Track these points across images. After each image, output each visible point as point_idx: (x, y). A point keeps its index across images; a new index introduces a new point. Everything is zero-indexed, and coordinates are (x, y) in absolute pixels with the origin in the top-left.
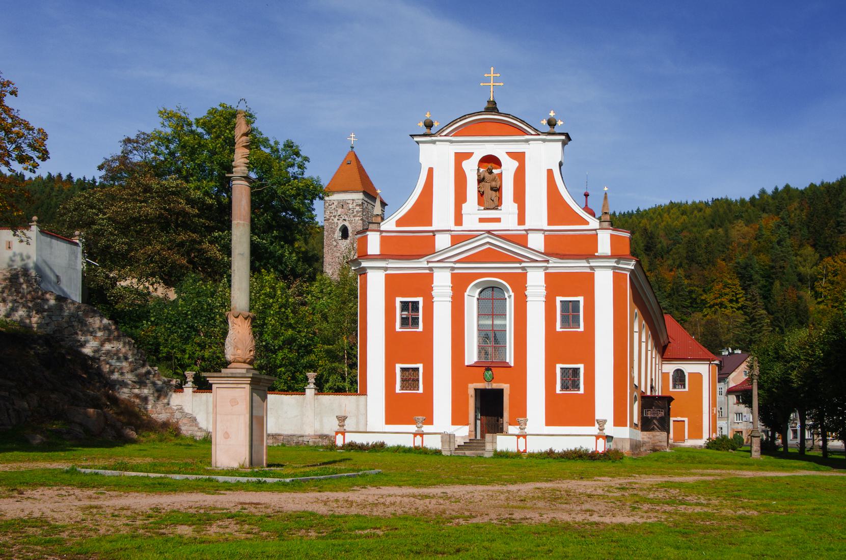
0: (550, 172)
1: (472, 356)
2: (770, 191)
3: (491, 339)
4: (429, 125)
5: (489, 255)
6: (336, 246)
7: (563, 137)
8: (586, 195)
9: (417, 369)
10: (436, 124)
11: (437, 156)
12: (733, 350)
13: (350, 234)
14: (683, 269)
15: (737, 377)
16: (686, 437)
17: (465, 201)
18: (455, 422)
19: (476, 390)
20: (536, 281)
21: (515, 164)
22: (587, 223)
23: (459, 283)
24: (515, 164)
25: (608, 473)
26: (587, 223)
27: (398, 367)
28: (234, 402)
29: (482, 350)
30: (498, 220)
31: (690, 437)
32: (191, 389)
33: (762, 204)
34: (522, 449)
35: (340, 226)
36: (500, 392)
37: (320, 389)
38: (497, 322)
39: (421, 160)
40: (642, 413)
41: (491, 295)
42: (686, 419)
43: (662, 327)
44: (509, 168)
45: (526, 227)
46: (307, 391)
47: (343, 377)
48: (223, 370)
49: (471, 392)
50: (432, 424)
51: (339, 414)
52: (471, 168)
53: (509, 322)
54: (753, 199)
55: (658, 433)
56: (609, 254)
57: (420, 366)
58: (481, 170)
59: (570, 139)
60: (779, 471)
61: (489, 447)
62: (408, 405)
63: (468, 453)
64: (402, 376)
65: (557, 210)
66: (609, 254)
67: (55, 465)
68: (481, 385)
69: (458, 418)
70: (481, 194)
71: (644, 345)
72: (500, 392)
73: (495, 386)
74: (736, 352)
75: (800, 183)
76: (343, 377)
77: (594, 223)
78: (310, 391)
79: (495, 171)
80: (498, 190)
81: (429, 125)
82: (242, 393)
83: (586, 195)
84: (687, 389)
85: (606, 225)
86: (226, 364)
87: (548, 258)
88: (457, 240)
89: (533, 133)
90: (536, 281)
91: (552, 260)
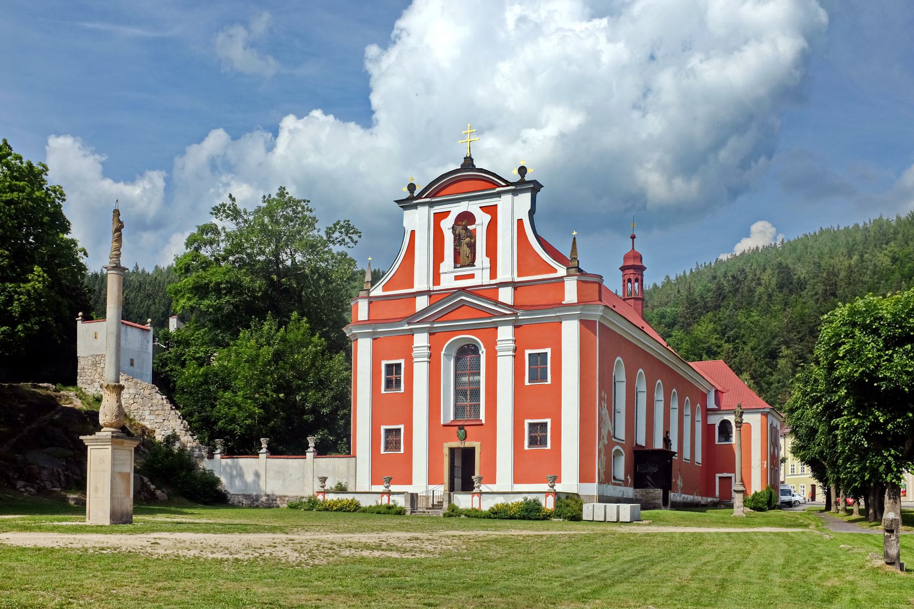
0: (520, 222)
1: (448, 414)
3: (467, 394)
4: (412, 187)
8: (633, 237)
17: (442, 260)
20: (505, 333)
21: (488, 218)
22: (555, 271)
24: (488, 218)
26: (555, 271)
29: (458, 410)
30: (472, 276)
31: (713, 495)
32: (312, 454)
34: (476, 506)
37: (273, 452)
38: (476, 378)
39: (405, 225)
40: (635, 469)
41: (466, 352)
44: (482, 219)
46: (308, 454)
47: (337, 442)
49: (446, 451)
50: (495, 483)
52: (447, 225)
55: (651, 490)
60: (722, 527)
62: (392, 463)
64: (386, 437)
68: (456, 444)
69: (433, 479)
73: (468, 444)
76: (337, 442)
77: (562, 271)
78: (310, 455)
79: (470, 227)
80: (472, 246)
83: (633, 237)
89: (503, 184)
91: (520, 312)
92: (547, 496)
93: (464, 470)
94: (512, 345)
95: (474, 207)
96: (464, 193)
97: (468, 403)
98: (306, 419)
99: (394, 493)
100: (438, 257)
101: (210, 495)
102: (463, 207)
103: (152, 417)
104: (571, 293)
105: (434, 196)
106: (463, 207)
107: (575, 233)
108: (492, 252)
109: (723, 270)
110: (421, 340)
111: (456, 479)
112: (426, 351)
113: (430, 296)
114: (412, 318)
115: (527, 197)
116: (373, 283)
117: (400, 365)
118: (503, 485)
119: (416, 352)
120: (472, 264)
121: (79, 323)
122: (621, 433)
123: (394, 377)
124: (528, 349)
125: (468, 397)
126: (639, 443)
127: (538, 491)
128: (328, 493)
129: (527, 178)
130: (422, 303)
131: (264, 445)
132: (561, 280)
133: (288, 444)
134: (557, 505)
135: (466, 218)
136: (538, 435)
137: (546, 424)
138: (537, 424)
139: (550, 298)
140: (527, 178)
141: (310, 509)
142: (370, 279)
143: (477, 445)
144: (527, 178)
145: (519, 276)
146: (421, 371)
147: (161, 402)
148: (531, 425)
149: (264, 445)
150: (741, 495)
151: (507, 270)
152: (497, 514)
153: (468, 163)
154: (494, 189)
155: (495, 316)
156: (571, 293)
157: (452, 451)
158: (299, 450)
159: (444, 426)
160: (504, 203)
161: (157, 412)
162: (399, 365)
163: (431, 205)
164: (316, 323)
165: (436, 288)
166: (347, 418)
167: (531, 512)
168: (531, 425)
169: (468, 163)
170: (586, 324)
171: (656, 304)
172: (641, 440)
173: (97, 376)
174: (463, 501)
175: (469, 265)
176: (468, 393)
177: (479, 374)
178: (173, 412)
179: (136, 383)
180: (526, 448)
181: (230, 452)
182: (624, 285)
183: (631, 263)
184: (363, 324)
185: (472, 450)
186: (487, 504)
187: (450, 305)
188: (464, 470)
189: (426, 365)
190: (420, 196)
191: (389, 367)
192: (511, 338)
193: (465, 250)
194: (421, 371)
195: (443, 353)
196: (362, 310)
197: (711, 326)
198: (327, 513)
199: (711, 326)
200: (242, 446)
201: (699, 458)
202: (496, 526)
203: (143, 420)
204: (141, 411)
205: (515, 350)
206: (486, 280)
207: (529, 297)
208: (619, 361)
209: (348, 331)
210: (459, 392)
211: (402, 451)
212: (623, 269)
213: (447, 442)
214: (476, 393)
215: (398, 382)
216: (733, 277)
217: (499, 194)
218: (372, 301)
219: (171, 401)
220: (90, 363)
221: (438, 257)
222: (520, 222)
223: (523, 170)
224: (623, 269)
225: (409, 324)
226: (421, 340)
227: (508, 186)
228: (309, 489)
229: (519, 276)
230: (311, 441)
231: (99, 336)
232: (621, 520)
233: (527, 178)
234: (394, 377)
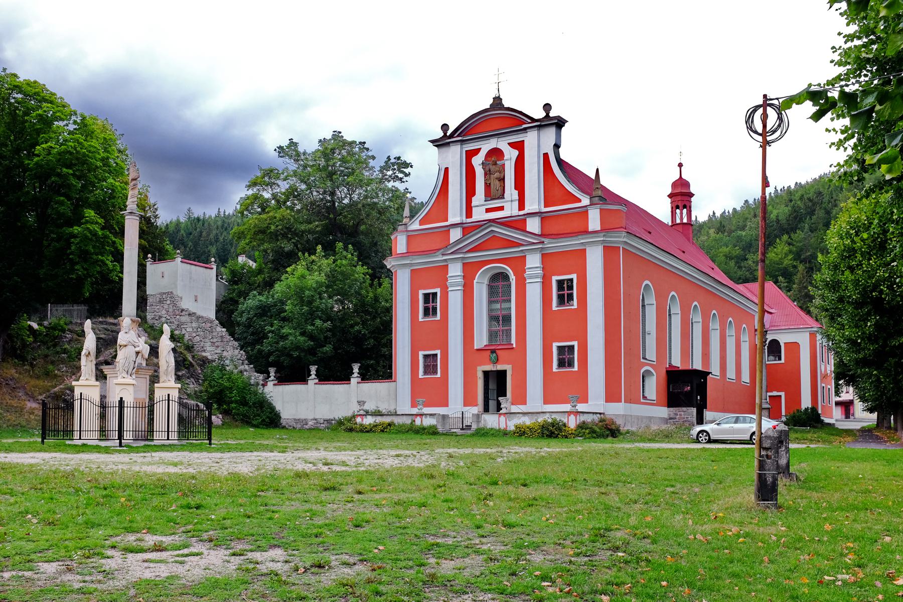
0: (546, 156)
1: (481, 340)
3: (499, 320)
4: (445, 127)
5: (494, 242)
8: (680, 165)
17: (474, 194)
20: (534, 262)
21: (516, 153)
22: (580, 201)
23: (470, 270)
24: (516, 153)
26: (580, 201)
27: (421, 354)
29: (492, 335)
30: (502, 208)
37: (324, 378)
38: (505, 305)
42: (782, 394)
44: (511, 155)
45: (526, 211)
46: (352, 380)
47: (379, 368)
49: (480, 375)
50: (525, 404)
51: (360, 400)
52: (477, 161)
56: (599, 229)
57: (438, 352)
62: (430, 389)
64: (425, 362)
66: (599, 229)
68: (488, 368)
69: (468, 401)
73: (500, 367)
76: (379, 368)
77: (585, 201)
78: (355, 380)
83: (680, 165)
84: (783, 361)
87: (543, 239)
88: (467, 230)
90: (534, 262)
91: (546, 240)
92: (569, 415)
95: (503, 144)
97: (501, 328)
98: (355, 346)
100: (470, 191)
101: (267, 418)
102: (492, 144)
104: (594, 221)
108: (520, 185)
109: (800, 193)
110: (455, 271)
111: (491, 402)
112: (460, 280)
115: (552, 131)
116: (412, 217)
118: (533, 404)
120: (502, 197)
121: (148, 264)
122: (651, 354)
123: (431, 305)
126: (674, 364)
127: (557, 410)
129: (552, 114)
130: (455, 235)
131: (313, 372)
133: (336, 373)
135: (496, 153)
136: (430, 363)
137: (573, 346)
138: (429, 355)
139: (575, 225)
141: (521, 435)
142: (408, 215)
143: (508, 368)
144: (551, 115)
145: (545, 207)
146: (455, 299)
148: (559, 348)
149: (313, 372)
151: (534, 201)
152: (521, 433)
153: (497, 101)
154: (521, 125)
155: (523, 245)
156: (594, 221)
157: (486, 374)
158: (345, 377)
160: (530, 139)
162: (435, 294)
163: (462, 142)
164: (363, 257)
165: (469, 220)
166: (389, 344)
167: (552, 431)
168: (559, 348)
169: (497, 101)
170: (610, 252)
171: (733, 228)
172: (677, 362)
173: (164, 312)
174: (491, 421)
175: (498, 198)
177: (510, 301)
180: (555, 370)
181: (282, 380)
182: (672, 212)
183: (678, 190)
184: (403, 256)
185: (505, 372)
186: (511, 425)
187: (486, 238)
190: (452, 136)
194: (455, 299)
196: (400, 243)
197: (787, 248)
199: (787, 248)
200: (293, 374)
201: (746, 378)
205: (544, 277)
206: (516, 212)
207: (554, 228)
208: (647, 285)
209: (389, 263)
210: (493, 318)
211: (439, 375)
212: (670, 196)
213: (480, 365)
214: (507, 319)
215: (435, 309)
216: (809, 199)
219: (232, 334)
221: (470, 191)
222: (546, 156)
223: (547, 107)
224: (670, 196)
226: (455, 271)
228: (341, 412)
229: (545, 207)
230: (356, 368)
231: (166, 275)
233: (552, 114)
234: (431, 305)
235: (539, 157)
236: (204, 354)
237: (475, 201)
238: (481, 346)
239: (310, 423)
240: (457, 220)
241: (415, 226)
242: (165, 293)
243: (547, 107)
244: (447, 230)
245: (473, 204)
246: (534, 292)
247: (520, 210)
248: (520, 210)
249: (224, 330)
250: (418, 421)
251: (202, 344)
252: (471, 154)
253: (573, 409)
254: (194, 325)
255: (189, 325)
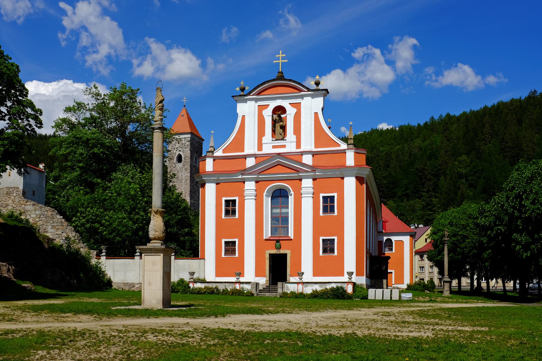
1: (267, 233)
2: (436, 117)
3: (280, 221)
4: (243, 90)
6: (175, 167)
7: (325, 92)
9: (235, 242)
10: (247, 88)
11: (247, 109)
12: (418, 225)
13: (183, 159)
14: (404, 171)
15: (421, 244)
16: (393, 283)
17: (264, 135)
18: (257, 275)
19: (270, 254)
21: (295, 110)
22: (339, 145)
24: (295, 110)
25: (177, 314)
26: (339, 145)
28: (154, 263)
29: (274, 230)
30: (284, 146)
33: (431, 127)
35: (177, 154)
36: (285, 255)
38: (284, 210)
39: (238, 111)
41: (280, 195)
43: (380, 211)
44: (291, 112)
48: (148, 244)
49: (267, 256)
52: (268, 114)
53: (291, 211)
54: (426, 124)
58: (275, 116)
59: (328, 93)
61: (280, 290)
63: (267, 294)
64: (323, 244)
65: (320, 136)
67: (95, 300)
68: (274, 251)
69: (258, 273)
70: (274, 131)
71: (371, 222)
72: (285, 255)
73: (282, 251)
74: (420, 226)
75: (457, 112)
79: (283, 116)
80: (284, 128)
81: (243, 90)
82: (159, 259)
85: (351, 146)
86: (149, 240)
93: (278, 268)
94: (312, 190)
96: (279, 94)
99: (243, 283)
103: (53, 230)
105: (258, 94)
106: (279, 103)
107: (351, 123)
108: (297, 131)
110: (250, 186)
113: (256, 158)
114: (244, 171)
117: (235, 200)
119: (246, 193)
123: (230, 208)
124: (224, 197)
125: (280, 222)
127: (333, 281)
128: (196, 282)
130: (250, 162)
132: (344, 152)
134: (354, 290)
136: (230, 247)
138: (230, 242)
140: (321, 87)
146: (250, 206)
147: (60, 220)
150: (448, 284)
151: (308, 143)
159: (266, 240)
161: (57, 227)
163: (256, 100)
173: (10, 202)
176: (280, 219)
178: (69, 228)
179: (41, 208)
181: (112, 254)
187: (269, 165)
188: (278, 268)
189: (253, 202)
191: (227, 201)
192: (312, 186)
193: (278, 130)
194: (250, 206)
195: (265, 194)
198: (212, 296)
202: (363, 305)
203: (47, 232)
204: (45, 227)
205: (313, 194)
207: (323, 161)
210: (274, 218)
214: (285, 219)
217: (302, 97)
218: (215, 159)
220: (5, 192)
221: (261, 133)
225: (242, 174)
227: (309, 91)
229: (315, 147)
232: (393, 299)
234: (230, 208)
235: (311, 115)
236: (47, 234)
237: (265, 140)
238: (267, 238)
239: (137, 286)
240: (252, 152)
241: (219, 153)
242: (12, 188)
243: (53, 127)
244: (245, 157)
245: (263, 142)
246: (307, 204)
247: (297, 148)
248: (297, 148)
249: (62, 217)
250: (238, 286)
251: (45, 227)
252: (262, 108)
253: (238, 281)
254: (37, 212)
255: (34, 212)
